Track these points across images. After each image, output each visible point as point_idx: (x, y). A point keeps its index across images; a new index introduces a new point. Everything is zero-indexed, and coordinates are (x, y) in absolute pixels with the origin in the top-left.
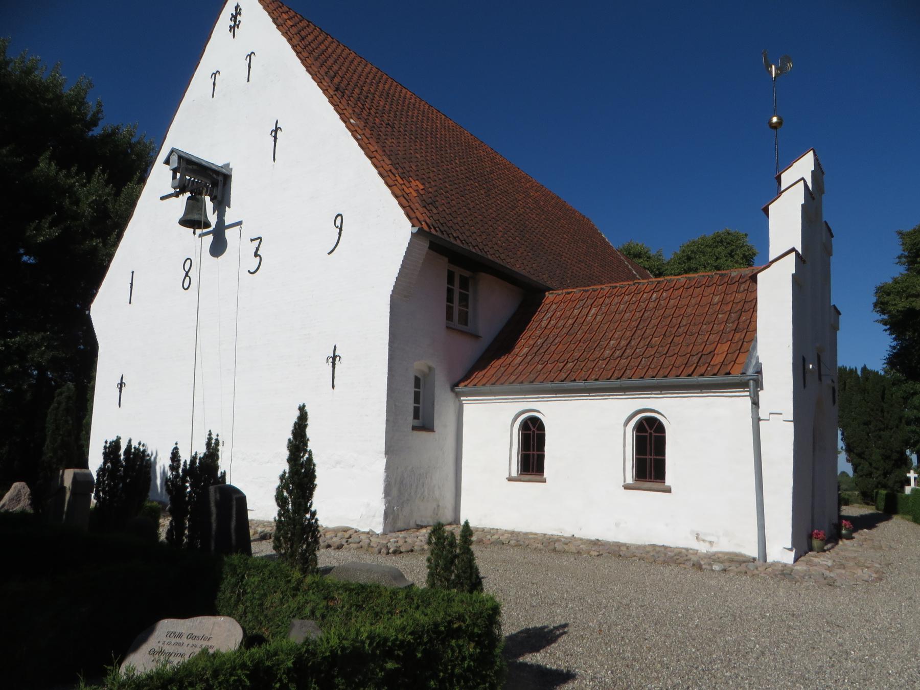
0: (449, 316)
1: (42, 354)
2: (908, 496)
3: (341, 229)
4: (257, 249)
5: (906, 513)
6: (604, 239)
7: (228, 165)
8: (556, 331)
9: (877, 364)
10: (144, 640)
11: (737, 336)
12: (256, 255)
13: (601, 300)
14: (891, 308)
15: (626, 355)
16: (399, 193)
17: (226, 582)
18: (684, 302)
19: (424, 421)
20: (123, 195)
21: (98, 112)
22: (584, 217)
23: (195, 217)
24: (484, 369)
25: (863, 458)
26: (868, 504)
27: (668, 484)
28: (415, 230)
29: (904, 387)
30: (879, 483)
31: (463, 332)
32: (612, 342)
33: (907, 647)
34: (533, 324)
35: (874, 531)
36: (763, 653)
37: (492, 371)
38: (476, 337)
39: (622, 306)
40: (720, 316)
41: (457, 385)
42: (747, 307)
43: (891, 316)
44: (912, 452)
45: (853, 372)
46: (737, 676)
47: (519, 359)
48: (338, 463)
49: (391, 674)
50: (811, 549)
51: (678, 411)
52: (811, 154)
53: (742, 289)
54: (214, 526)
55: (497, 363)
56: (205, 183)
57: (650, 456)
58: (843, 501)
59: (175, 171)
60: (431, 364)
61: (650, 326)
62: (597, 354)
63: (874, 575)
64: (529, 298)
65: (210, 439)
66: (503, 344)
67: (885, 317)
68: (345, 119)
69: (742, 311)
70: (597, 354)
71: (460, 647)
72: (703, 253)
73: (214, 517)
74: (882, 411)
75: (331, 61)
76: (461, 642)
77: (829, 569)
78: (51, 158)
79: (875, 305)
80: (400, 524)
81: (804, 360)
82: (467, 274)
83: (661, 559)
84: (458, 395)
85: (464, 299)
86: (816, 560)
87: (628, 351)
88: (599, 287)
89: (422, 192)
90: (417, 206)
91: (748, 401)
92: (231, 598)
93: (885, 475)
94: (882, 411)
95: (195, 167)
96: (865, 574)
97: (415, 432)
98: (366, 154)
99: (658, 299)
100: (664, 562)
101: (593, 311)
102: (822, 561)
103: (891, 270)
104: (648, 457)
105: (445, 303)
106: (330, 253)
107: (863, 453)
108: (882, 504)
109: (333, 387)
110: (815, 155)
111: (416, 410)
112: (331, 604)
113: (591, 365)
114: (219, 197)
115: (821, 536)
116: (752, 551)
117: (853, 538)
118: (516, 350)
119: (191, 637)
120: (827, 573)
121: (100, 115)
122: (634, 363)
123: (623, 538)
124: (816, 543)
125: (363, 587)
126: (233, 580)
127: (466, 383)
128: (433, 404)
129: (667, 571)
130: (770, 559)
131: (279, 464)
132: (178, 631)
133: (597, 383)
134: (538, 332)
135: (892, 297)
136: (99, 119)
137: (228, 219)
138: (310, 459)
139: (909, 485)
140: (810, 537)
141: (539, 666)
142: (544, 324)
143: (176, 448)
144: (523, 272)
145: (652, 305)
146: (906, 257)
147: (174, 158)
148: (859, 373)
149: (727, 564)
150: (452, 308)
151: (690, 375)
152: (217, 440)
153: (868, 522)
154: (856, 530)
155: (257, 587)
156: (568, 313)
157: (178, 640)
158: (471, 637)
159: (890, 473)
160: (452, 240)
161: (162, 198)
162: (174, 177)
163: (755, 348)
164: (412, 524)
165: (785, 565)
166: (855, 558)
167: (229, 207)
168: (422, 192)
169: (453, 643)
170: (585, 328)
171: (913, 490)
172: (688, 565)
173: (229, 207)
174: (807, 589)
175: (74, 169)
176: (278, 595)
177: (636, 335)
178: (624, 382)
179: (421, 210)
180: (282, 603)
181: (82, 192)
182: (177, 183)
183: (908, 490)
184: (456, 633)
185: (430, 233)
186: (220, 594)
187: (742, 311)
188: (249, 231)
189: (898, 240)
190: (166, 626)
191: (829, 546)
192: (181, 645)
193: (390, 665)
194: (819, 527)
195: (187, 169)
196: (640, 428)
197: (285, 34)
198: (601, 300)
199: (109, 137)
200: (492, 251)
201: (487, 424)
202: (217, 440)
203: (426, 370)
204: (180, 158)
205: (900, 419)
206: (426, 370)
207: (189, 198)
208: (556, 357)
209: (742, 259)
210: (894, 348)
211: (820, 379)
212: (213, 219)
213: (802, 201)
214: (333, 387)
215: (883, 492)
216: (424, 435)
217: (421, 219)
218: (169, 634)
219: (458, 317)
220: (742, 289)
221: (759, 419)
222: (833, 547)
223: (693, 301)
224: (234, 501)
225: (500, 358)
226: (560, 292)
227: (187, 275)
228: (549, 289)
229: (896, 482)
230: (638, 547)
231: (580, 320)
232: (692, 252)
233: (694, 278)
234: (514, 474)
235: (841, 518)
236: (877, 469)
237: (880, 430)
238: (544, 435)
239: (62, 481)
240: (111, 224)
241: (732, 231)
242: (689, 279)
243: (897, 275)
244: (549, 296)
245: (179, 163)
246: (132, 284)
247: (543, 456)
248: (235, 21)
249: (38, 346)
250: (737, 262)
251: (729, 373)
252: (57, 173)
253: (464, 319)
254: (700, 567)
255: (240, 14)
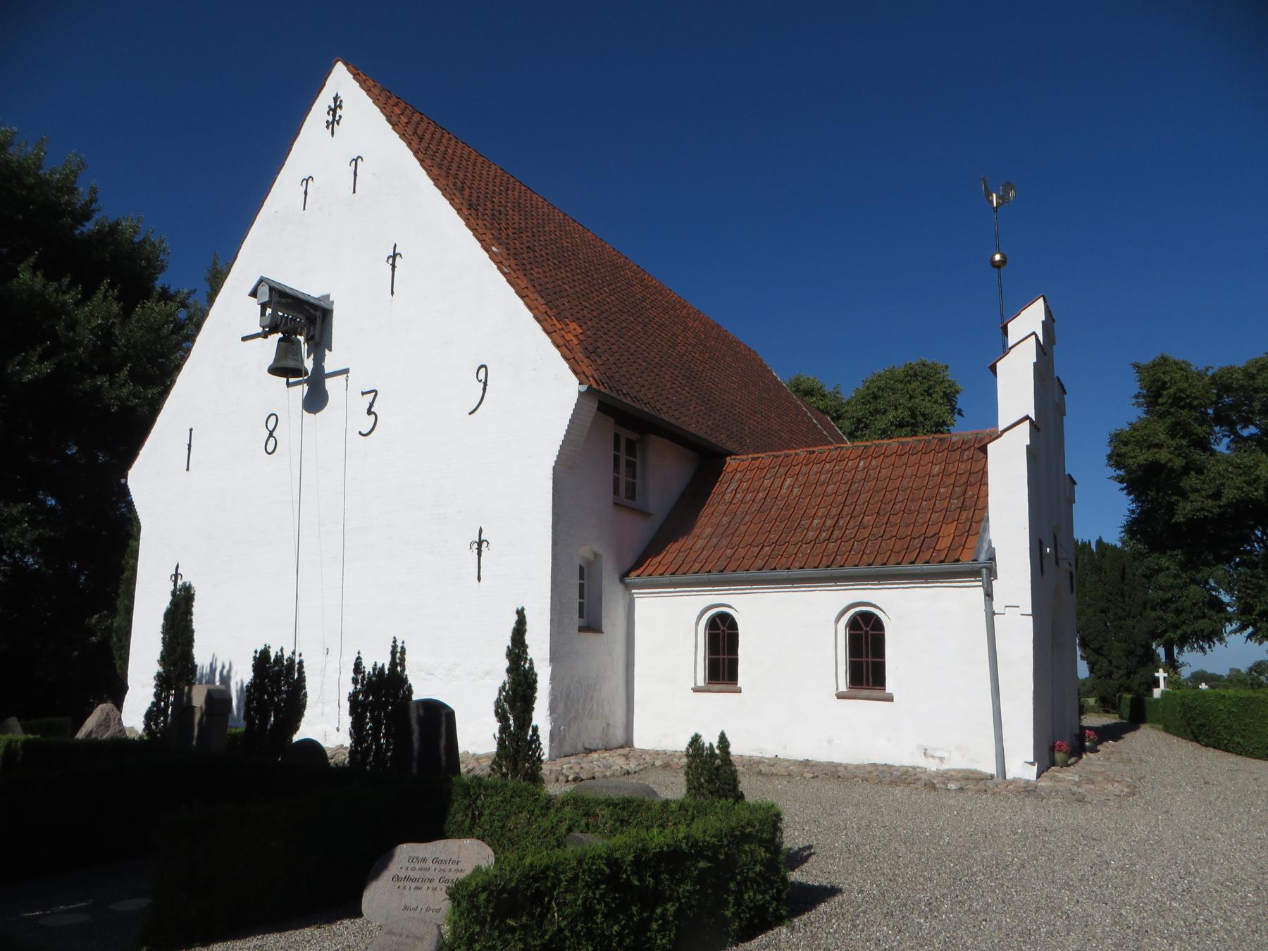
0: (616, 492)
1: (23, 533)
2: (1157, 701)
3: (485, 384)
4: (371, 405)
5: (1155, 721)
6: (775, 378)
7: (328, 296)
8: (745, 507)
9: (1114, 536)
10: (384, 866)
11: (964, 514)
12: (369, 412)
13: (797, 468)
14: (1130, 461)
15: (834, 537)
16: (561, 342)
17: (456, 805)
18: (898, 472)
19: (591, 625)
20: (134, 317)
21: (92, 201)
22: (749, 350)
23: (291, 363)
24: (658, 554)
25: (1102, 655)
26: (1108, 712)
27: (871, 692)
28: (584, 388)
29: (1146, 562)
30: (1121, 686)
31: (632, 509)
32: (816, 521)
33: (1167, 856)
34: (713, 498)
35: (1121, 742)
36: (1023, 866)
37: (670, 558)
38: (647, 514)
39: (823, 477)
40: (942, 490)
41: (627, 574)
42: (972, 479)
43: (1129, 471)
44: (1158, 645)
45: (1086, 546)
46: (1002, 885)
47: (701, 543)
48: (487, 673)
49: (702, 870)
50: (1053, 764)
51: (899, 605)
52: (1041, 302)
53: (965, 457)
54: (416, 745)
55: (674, 548)
56: (299, 323)
57: (722, 655)
58: (1082, 710)
59: (264, 306)
60: (597, 549)
61: (860, 502)
62: (798, 536)
63: (1126, 790)
64: (707, 464)
65: (394, 647)
66: (679, 521)
67: (1122, 472)
68: (487, 248)
69: (967, 484)
70: (798, 536)
71: (752, 852)
72: (894, 390)
73: (416, 735)
74: (1123, 595)
75: (455, 166)
76: (753, 847)
77: (1077, 784)
78: (35, 268)
79: (1110, 457)
80: (567, 748)
81: (1041, 543)
82: (634, 436)
83: (888, 779)
84: (628, 587)
85: (631, 466)
86: (1060, 775)
87: (836, 532)
88: (792, 452)
89: (582, 337)
90: (580, 356)
91: (981, 591)
92: (463, 821)
93: (1128, 675)
94: (1123, 595)
95: (289, 301)
96: (1116, 788)
97: (582, 634)
98: (517, 292)
99: (867, 468)
100: (891, 783)
101: (788, 482)
102: (1067, 776)
103: (1127, 412)
104: (864, 659)
105: (612, 474)
106: (471, 413)
107: (1101, 648)
108: (1126, 711)
109: (479, 579)
110: (1048, 312)
111: (584, 606)
112: (591, 820)
113: (792, 550)
114: (317, 338)
115: (1065, 748)
116: (990, 768)
117: (1098, 751)
118: (696, 530)
119: (436, 861)
120: (1075, 789)
121: (94, 206)
122: (846, 547)
123: (836, 758)
124: (1059, 756)
125: (629, 801)
126: (466, 802)
127: (638, 572)
128: (601, 599)
129: (897, 791)
130: (1009, 776)
131: (498, 673)
132: (421, 856)
133: (802, 572)
134: (722, 508)
135: (1130, 447)
136: (93, 211)
137: (329, 366)
138: (531, 668)
139: (1158, 686)
140: (1052, 749)
141: (800, 884)
142: (728, 497)
143: (359, 658)
144: (701, 434)
145: (859, 476)
146: (1144, 397)
147: (264, 290)
148: (1093, 547)
149: (963, 783)
150: (634, 485)
151: (913, 563)
152: (403, 648)
153: (1112, 733)
154: (1100, 742)
155: (497, 809)
156: (757, 484)
157: (424, 865)
158: (762, 842)
159: (1134, 673)
160: (622, 398)
161: (244, 339)
162: (263, 313)
163: (986, 529)
164: (580, 747)
165: (1027, 782)
166: (1103, 773)
167: (330, 350)
168: (582, 337)
169: (746, 847)
170: (780, 503)
171: (1163, 692)
172: (919, 785)
173: (330, 350)
174: (1056, 805)
175: (66, 281)
176: (524, 814)
177: (844, 513)
178: (835, 570)
179: (586, 361)
180: (529, 823)
181: (82, 313)
182: (267, 321)
183: (1157, 693)
184: (747, 838)
185: (599, 391)
186: (450, 818)
187: (967, 484)
188: (359, 380)
189: (1133, 375)
190: (404, 851)
191: (1073, 760)
192: (427, 870)
193: (702, 864)
194: (1061, 741)
195: (279, 304)
196: (853, 625)
197: (403, 136)
198: (797, 468)
199: (110, 234)
200: (665, 409)
201: (666, 623)
202: (403, 648)
203: (591, 557)
204: (272, 289)
205: (1145, 604)
206: (591, 557)
207: (280, 340)
208: (748, 540)
209: (942, 397)
210: (1133, 512)
211: (1057, 564)
212: (309, 364)
213: (1033, 358)
214: (479, 579)
215: (1128, 696)
216: (590, 637)
217: (589, 374)
218: (411, 859)
219: (626, 495)
220: (965, 457)
221: (994, 613)
222: (1076, 762)
223: (909, 471)
224: (438, 718)
225: (676, 541)
226: (744, 457)
227: (271, 435)
228: (730, 454)
229: (1141, 684)
230: (858, 767)
231: (773, 494)
232: (879, 388)
233: (908, 443)
234: (701, 683)
235: (1082, 728)
236: (1118, 668)
237: (1120, 619)
238: (736, 636)
239: (190, 699)
240: (156, 363)
241: (929, 362)
242: (902, 443)
243: (1134, 420)
244: (731, 462)
245: (271, 296)
246: (190, 446)
247: (736, 661)
248: (334, 116)
249: (16, 521)
250: (936, 402)
251: (958, 560)
252: (45, 286)
253: (631, 494)
254: (934, 787)
255: (341, 107)
